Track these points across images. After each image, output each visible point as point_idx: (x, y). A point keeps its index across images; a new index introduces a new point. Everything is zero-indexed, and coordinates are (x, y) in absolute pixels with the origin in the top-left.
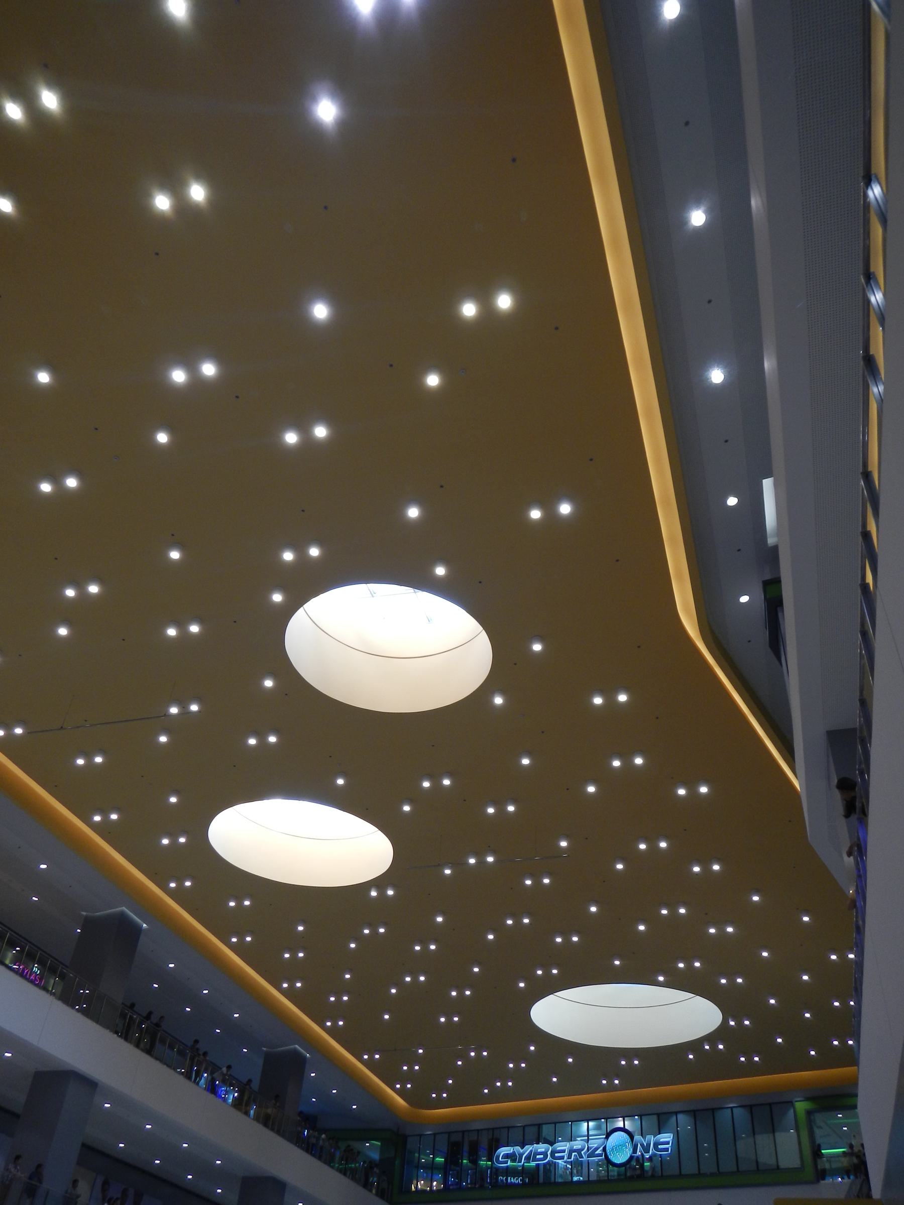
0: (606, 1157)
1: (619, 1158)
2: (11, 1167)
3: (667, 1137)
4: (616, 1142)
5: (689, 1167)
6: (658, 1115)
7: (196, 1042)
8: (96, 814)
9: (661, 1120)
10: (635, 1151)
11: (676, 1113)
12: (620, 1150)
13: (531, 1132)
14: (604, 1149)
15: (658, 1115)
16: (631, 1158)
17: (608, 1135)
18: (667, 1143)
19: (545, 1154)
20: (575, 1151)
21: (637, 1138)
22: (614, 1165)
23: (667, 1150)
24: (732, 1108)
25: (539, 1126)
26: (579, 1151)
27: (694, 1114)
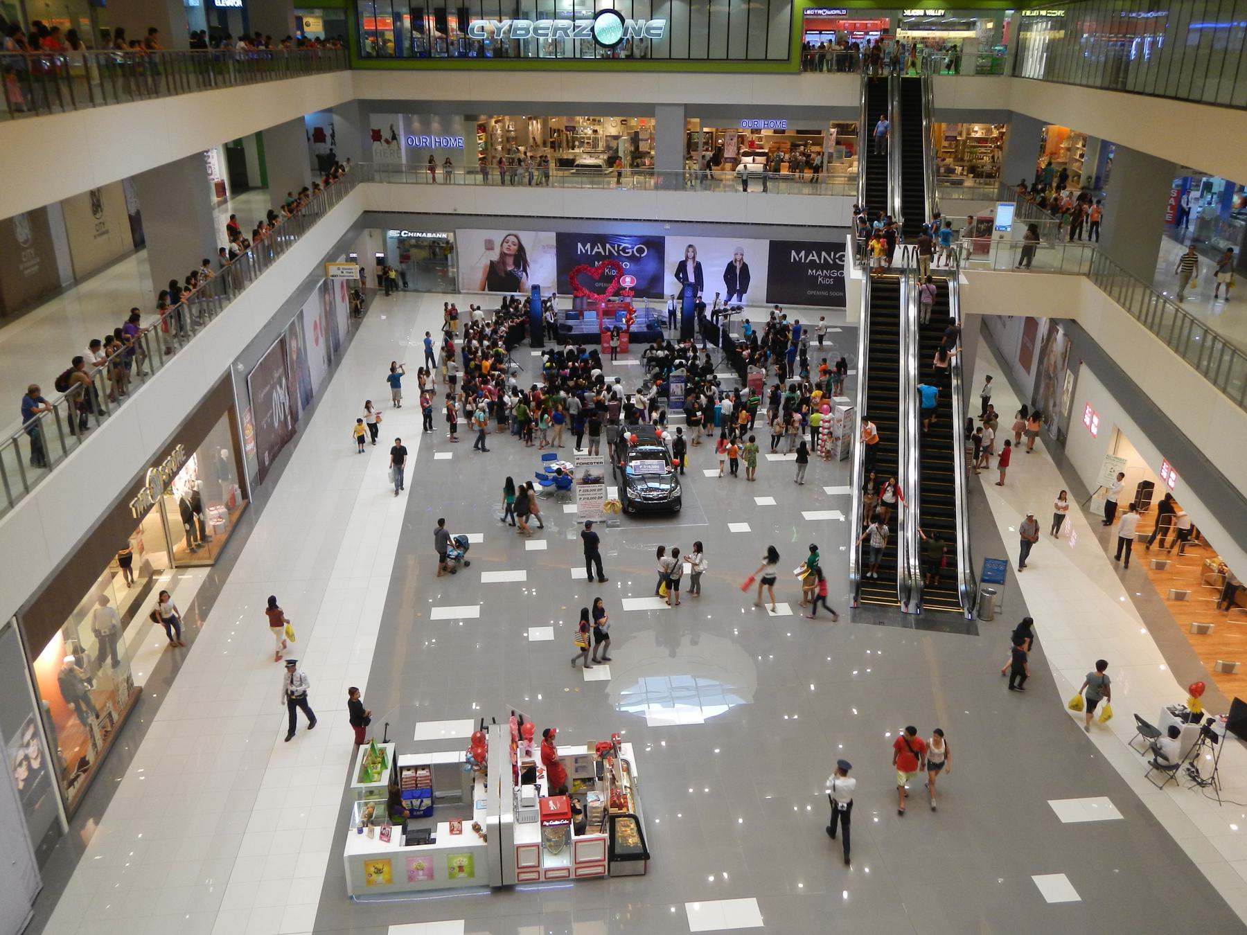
0: (594, 37)
1: (609, 39)
3: (659, 23)
10: (625, 33)
14: (592, 29)
16: (621, 39)
17: (596, 16)
21: (629, 22)
26: (565, 30)
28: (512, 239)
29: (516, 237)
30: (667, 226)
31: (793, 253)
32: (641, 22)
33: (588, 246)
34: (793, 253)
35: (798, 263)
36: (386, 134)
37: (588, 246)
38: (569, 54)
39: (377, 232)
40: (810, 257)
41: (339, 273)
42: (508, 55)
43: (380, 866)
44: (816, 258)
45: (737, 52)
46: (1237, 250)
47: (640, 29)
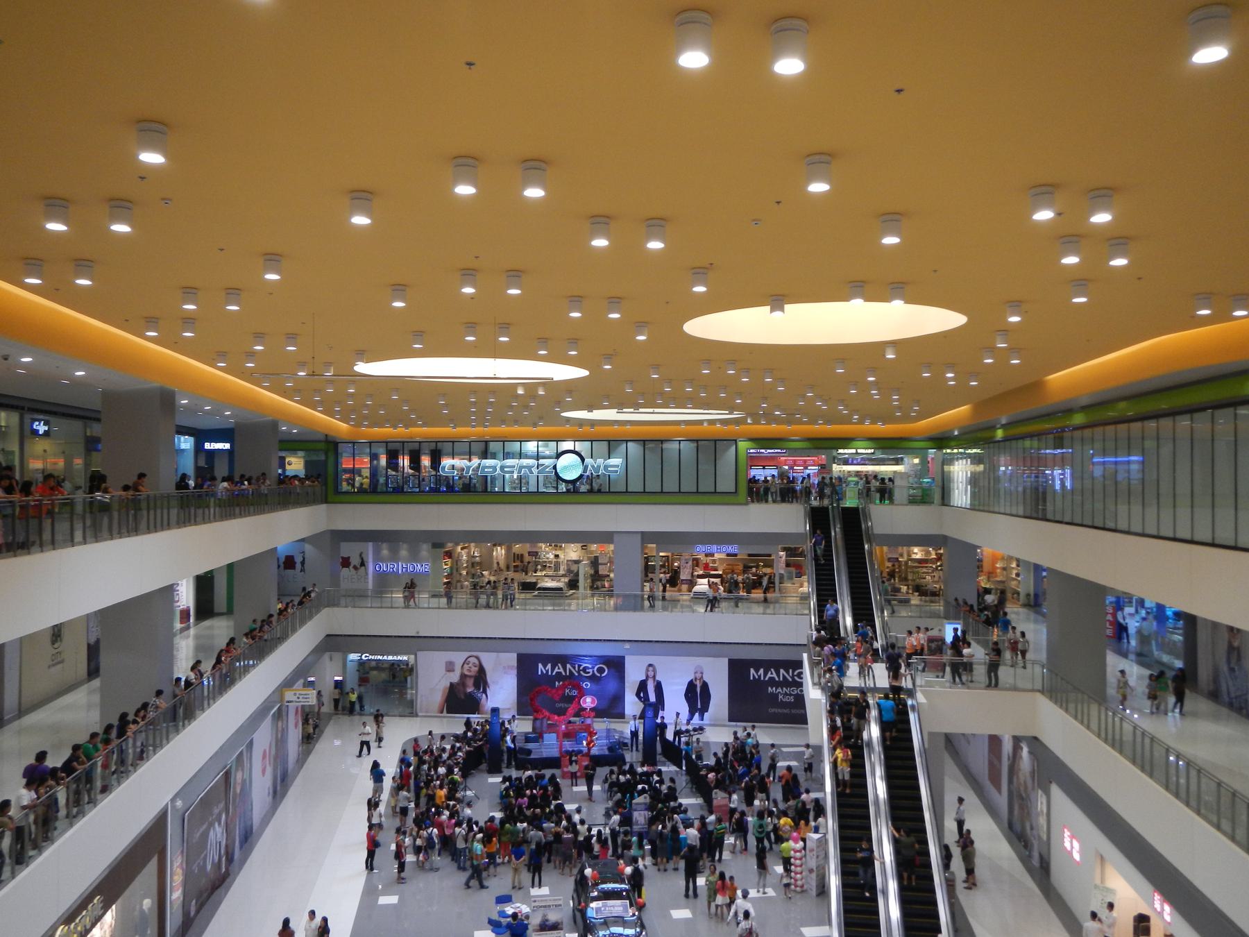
3: (616, 461)
10: (585, 470)
12: (570, 468)
14: (555, 467)
16: (581, 476)
21: (588, 461)
28: (473, 660)
29: (477, 658)
32: (600, 461)
33: (761, 671)
34: (752, 671)
36: (355, 561)
40: (769, 675)
42: (474, 490)
44: (774, 675)
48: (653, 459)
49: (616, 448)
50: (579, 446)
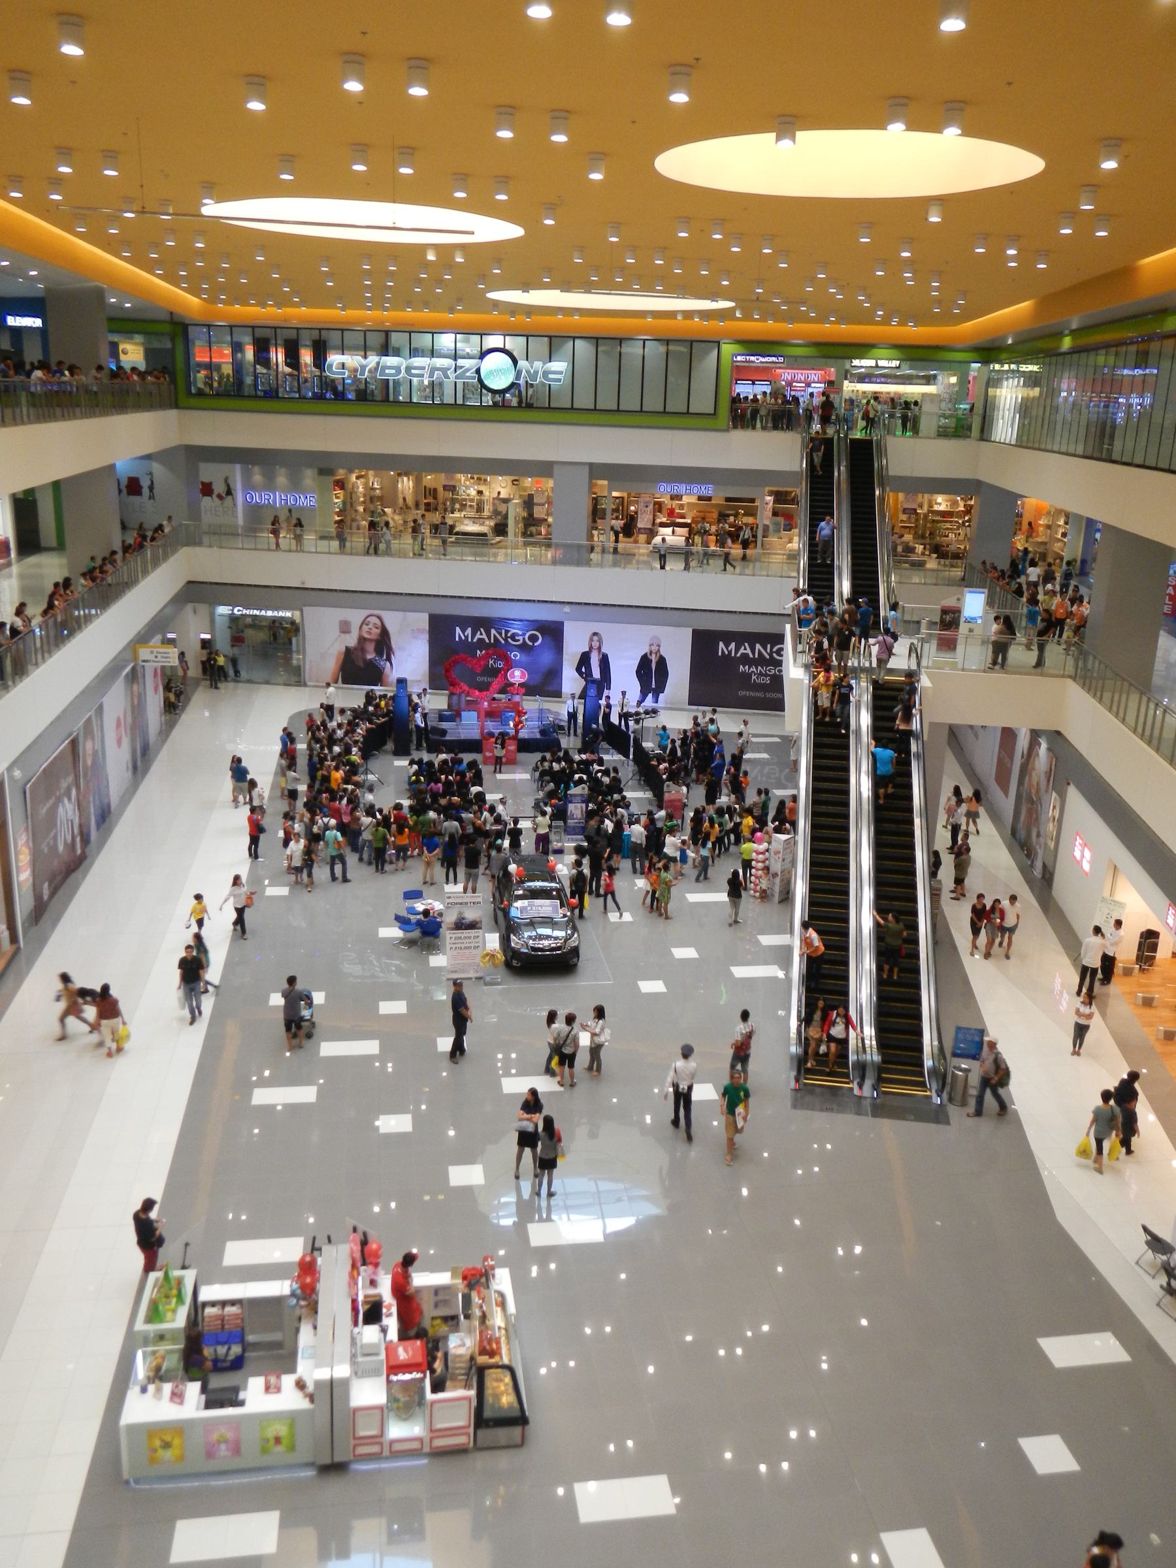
1: (499, 382)
2: (298, 619)
3: (559, 366)
4: (14, 194)
5: (584, 400)
6: (550, 337)
7: (984, 563)
8: (945, 13)
9: (554, 341)
10: (518, 376)
11: (574, 338)
12: (498, 373)
13: (375, 340)
14: (478, 371)
15: (550, 337)
16: (513, 385)
18: (561, 373)
19: (398, 369)
20: (438, 369)
21: (522, 363)
22: (489, 390)
23: (559, 380)
24: (644, 340)
25: (387, 333)
26: (444, 370)
27: (596, 340)
28: (374, 620)
29: (379, 618)
30: (567, 609)
31: (721, 645)
32: (538, 364)
33: (733, 646)
34: (721, 645)
35: (727, 657)
36: (219, 488)
37: (733, 646)
38: (449, 399)
39: (203, 608)
41: (151, 657)
42: (374, 398)
43: (168, 1438)
45: (653, 402)
46: (223, 610)
47: (536, 372)
48: (608, 365)
49: (560, 346)
50: (511, 343)
